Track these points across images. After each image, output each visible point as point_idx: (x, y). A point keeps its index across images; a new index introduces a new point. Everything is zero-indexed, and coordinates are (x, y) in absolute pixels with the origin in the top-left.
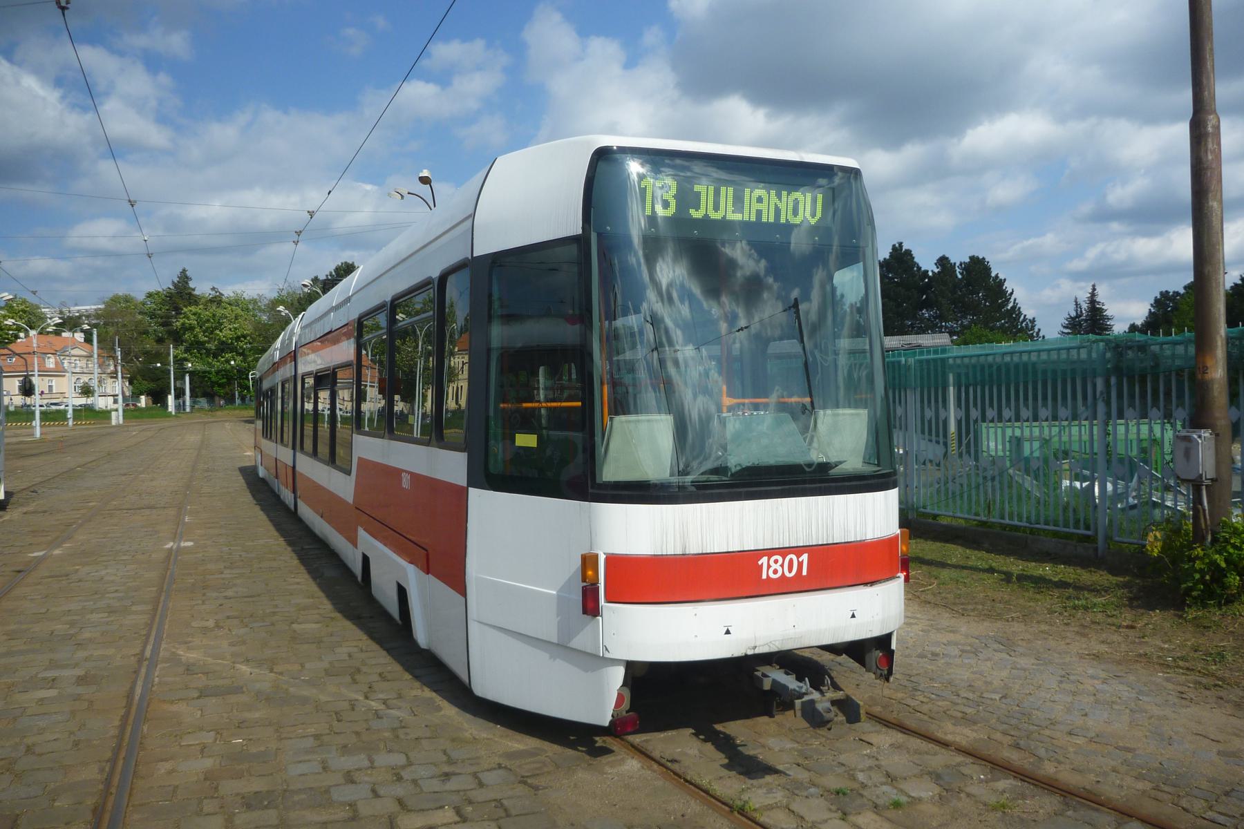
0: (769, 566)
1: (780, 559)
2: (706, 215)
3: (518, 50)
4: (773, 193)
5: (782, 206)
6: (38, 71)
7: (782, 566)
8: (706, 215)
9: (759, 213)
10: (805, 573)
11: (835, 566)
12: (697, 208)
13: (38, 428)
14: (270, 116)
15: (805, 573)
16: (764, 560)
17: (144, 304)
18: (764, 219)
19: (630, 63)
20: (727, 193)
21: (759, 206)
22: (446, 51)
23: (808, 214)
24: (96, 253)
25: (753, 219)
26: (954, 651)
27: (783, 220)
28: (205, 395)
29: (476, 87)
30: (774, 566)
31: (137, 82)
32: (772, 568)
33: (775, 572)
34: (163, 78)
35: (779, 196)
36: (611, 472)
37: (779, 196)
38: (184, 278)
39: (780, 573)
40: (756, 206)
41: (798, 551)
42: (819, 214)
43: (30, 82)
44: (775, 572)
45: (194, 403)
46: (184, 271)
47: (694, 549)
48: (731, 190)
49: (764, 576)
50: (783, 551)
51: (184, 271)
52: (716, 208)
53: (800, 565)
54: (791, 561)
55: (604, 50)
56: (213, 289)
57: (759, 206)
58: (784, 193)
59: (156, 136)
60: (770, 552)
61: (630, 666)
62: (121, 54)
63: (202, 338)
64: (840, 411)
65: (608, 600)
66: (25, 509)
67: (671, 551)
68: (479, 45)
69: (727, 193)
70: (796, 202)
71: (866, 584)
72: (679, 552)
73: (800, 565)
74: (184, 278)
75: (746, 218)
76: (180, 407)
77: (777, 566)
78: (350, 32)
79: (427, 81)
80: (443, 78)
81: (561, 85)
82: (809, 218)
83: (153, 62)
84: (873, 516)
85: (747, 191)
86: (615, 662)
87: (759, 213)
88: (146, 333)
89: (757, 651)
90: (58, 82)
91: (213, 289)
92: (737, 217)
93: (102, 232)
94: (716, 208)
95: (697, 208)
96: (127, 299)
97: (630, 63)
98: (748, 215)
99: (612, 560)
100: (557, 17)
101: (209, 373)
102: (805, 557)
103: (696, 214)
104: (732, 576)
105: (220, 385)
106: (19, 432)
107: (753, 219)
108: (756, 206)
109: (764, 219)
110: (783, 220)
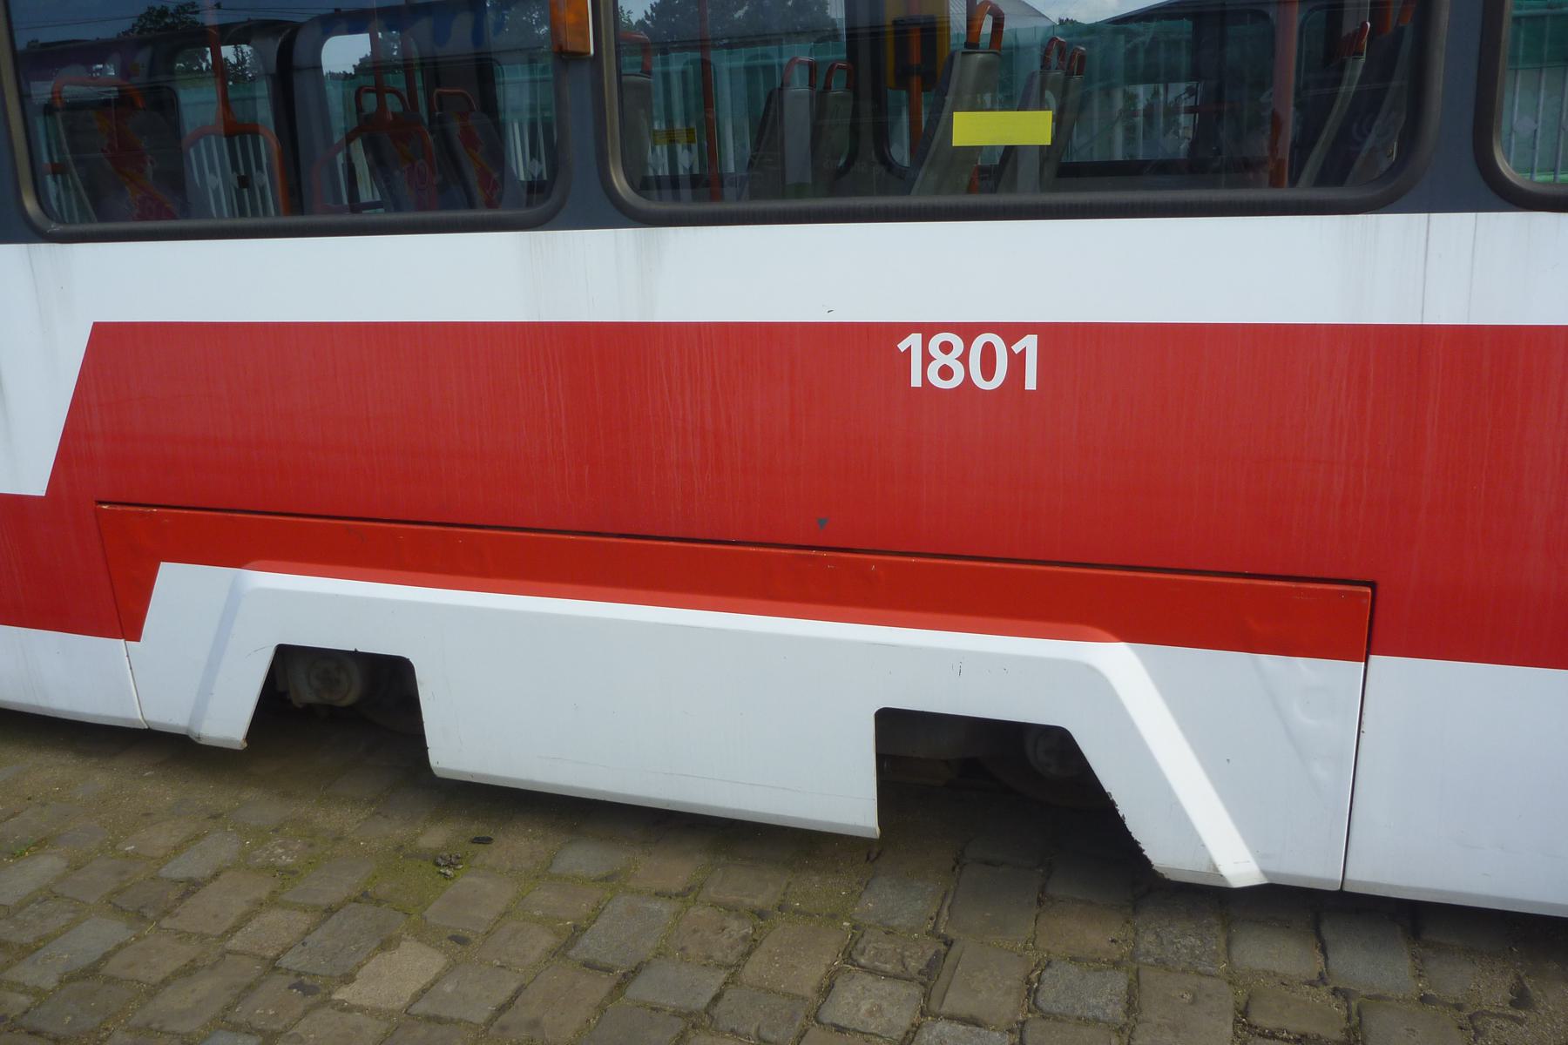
0: (927, 359)
7: (964, 359)
10: (1031, 383)
15: (1031, 383)
16: (913, 341)
30: (940, 359)
49: (916, 381)
53: (1017, 362)
73: (1017, 362)
77: (951, 360)
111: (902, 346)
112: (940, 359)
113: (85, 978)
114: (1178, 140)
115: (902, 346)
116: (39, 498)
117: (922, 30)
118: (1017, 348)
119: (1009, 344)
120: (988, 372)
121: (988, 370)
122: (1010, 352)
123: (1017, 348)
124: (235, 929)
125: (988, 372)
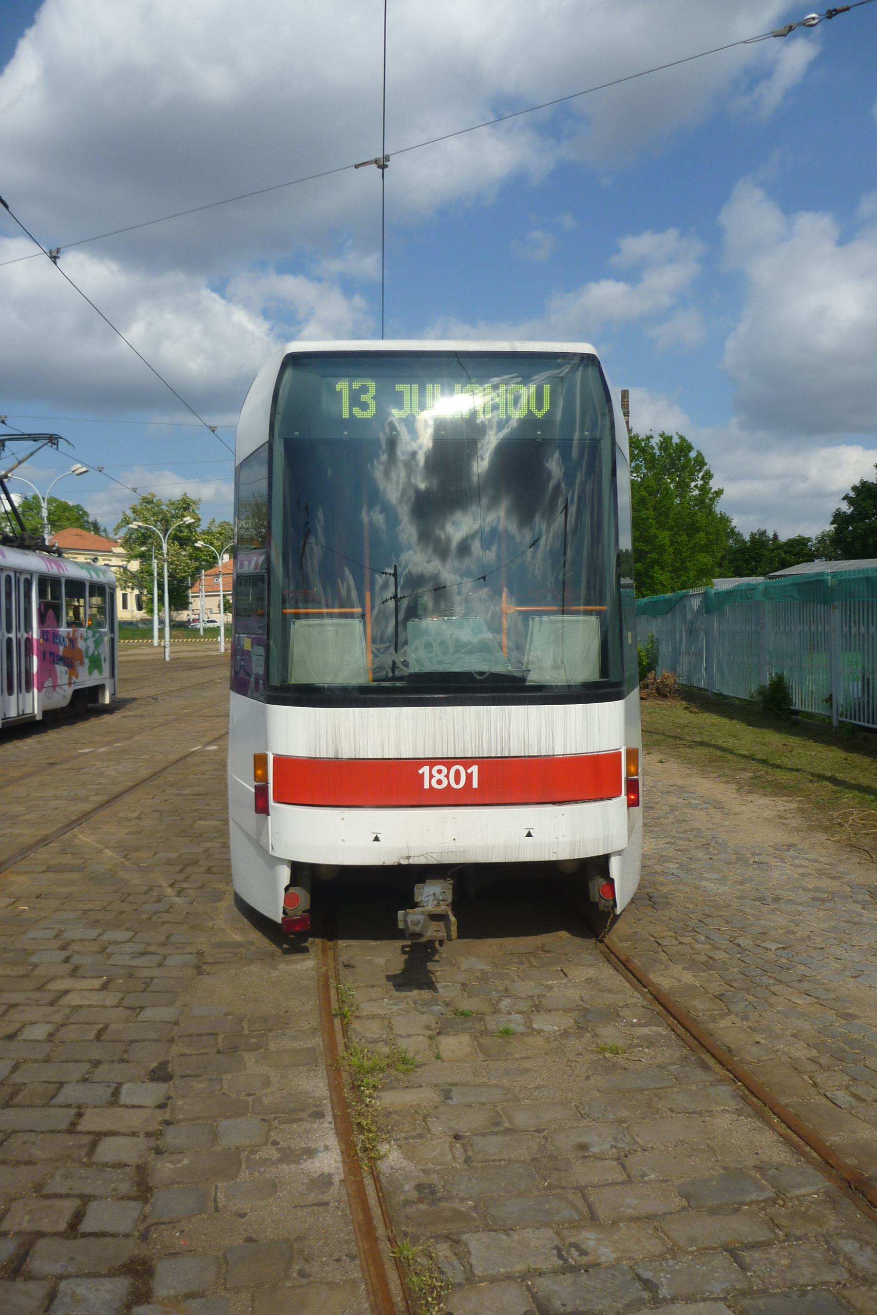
0: (431, 776)
1: (445, 770)
3: (714, 236)
6: (247, 305)
7: (447, 776)
10: (475, 785)
12: (400, 406)
13: (223, 643)
15: (475, 785)
16: (425, 770)
19: (844, 239)
22: (637, 245)
26: (804, 897)
29: (667, 280)
30: (437, 776)
32: (434, 779)
33: (439, 782)
34: (358, 301)
36: (298, 676)
39: (445, 784)
41: (467, 762)
42: (546, 406)
43: (240, 316)
47: (347, 752)
49: (426, 786)
50: (448, 762)
53: (469, 777)
54: (457, 773)
55: (815, 226)
60: (432, 762)
61: (297, 868)
62: (320, 280)
65: (277, 800)
66: (123, 714)
67: (323, 755)
68: (672, 234)
71: (554, 803)
72: (331, 755)
73: (469, 777)
77: (442, 777)
78: (537, 234)
79: (617, 280)
80: (631, 275)
81: (763, 271)
82: (535, 411)
83: (348, 286)
84: (599, 728)
86: (281, 861)
89: (412, 861)
90: (266, 314)
95: (400, 406)
97: (844, 239)
99: (280, 760)
100: (759, 194)
102: (474, 769)
104: (390, 783)
106: (210, 646)
111: (420, 772)
112: (437, 776)
113: (307, 531)
114: (585, 670)
115: (420, 772)
116: (413, 898)
117: (241, 585)
118: (469, 771)
119: (466, 769)
120: (457, 781)
121: (457, 780)
122: (466, 773)
123: (469, 771)
124: (613, 1184)
125: (457, 781)
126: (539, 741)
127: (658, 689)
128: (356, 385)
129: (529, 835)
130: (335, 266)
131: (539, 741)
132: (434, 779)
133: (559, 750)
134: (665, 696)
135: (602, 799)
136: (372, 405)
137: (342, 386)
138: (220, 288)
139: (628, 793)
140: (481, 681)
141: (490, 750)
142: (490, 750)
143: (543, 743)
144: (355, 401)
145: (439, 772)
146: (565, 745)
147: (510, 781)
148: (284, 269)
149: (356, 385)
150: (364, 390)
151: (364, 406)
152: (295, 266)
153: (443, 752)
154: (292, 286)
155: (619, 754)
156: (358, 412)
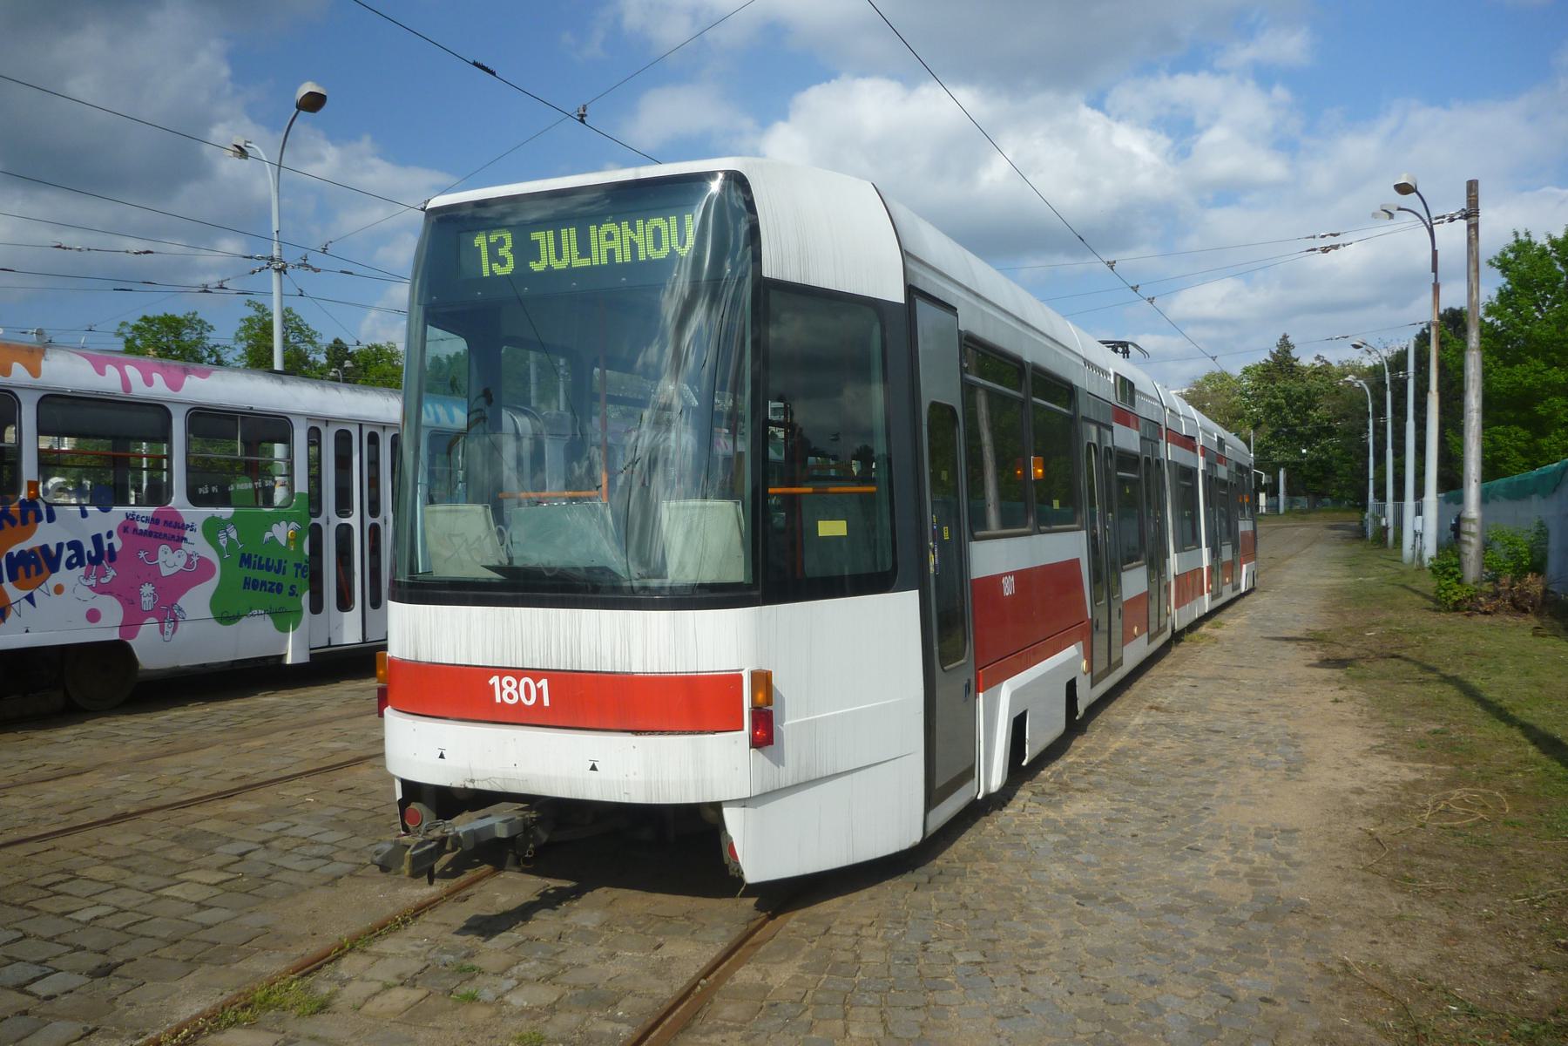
0: (502, 689)
2: (549, 266)
4: (625, 224)
5: (639, 239)
7: (517, 689)
8: (549, 266)
9: (611, 253)
10: (546, 703)
11: (459, 693)
12: (538, 259)
14: (1422, 116)
15: (546, 703)
16: (495, 680)
17: (1239, 381)
18: (618, 260)
20: (569, 235)
21: (610, 245)
23: (675, 244)
24: (1206, 322)
25: (605, 261)
27: (642, 257)
28: (1307, 493)
30: (511, 689)
31: (1251, 106)
32: (506, 691)
33: (510, 696)
34: (1280, 93)
35: (633, 228)
37: (633, 228)
38: (1285, 346)
40: (605, 245)
41: (537, 674)
44: (510, 696)
45: (1290, 504)
46: (1285, 337)
47: (424, 657)
48: (573, 231)
49: (498, 700)
50: (518, 672)
51: (1285, 337)
52: (559, 256)
53: (539, 692)
56: (1318, 358)
57: (610, 245)
58: (639, 223)
59: (1272, 168)
60: (502, 671)
63: (1291, 419)
64: (708, 503)
69: (569, 235)
70: (657, 231)
73: (539, 692)
74: (1285, 346)
75: (595, 262)
76: (1272, 508)
77: (511, 689)
83: (1264, 76)
85: (593, 228)
87: (611, 253)
88: (1241, 416)
91: (1318, 358)
92: (585, 262)
93: (1208, 298)
94: (559, 256)
95: (538, 259)
96: (1223, 377)
98: (598, 258)
101: (1301, 464)
102: (544, 683)
103: (537, 267)
105: (1314, 480)
107: (605, 261)
108: (605, 245)
109: (618, 260)
110: (642, 257)
120: (528, 697)
126: (613, 653)
127: (1512, 600)
128: (493, 239)
129: (593, 768)
130: (1244, 54)
131: (613, 653)
132: (506, 691)
133: (637, 668)
134: (1525, 611)
135: (701, 732)
136: (510, 258)
137: (480, 241)
138: (1097, 103)
139: (755, 725)
140: (550, 578)
141: (559, 662)
142: (559, 662)
143: (617, 656)
144: (494, 257)
145: (509, 684)
146: (644, 661)
147: (584, 701)
148: (1175, 69)
149: (493, 239)
150: (501, 242)
151: (502, 262)
152: (1193, 61)
153: (614, 661)
154: (1187, 88)
155: (740, 678)
156: (499, 270)
